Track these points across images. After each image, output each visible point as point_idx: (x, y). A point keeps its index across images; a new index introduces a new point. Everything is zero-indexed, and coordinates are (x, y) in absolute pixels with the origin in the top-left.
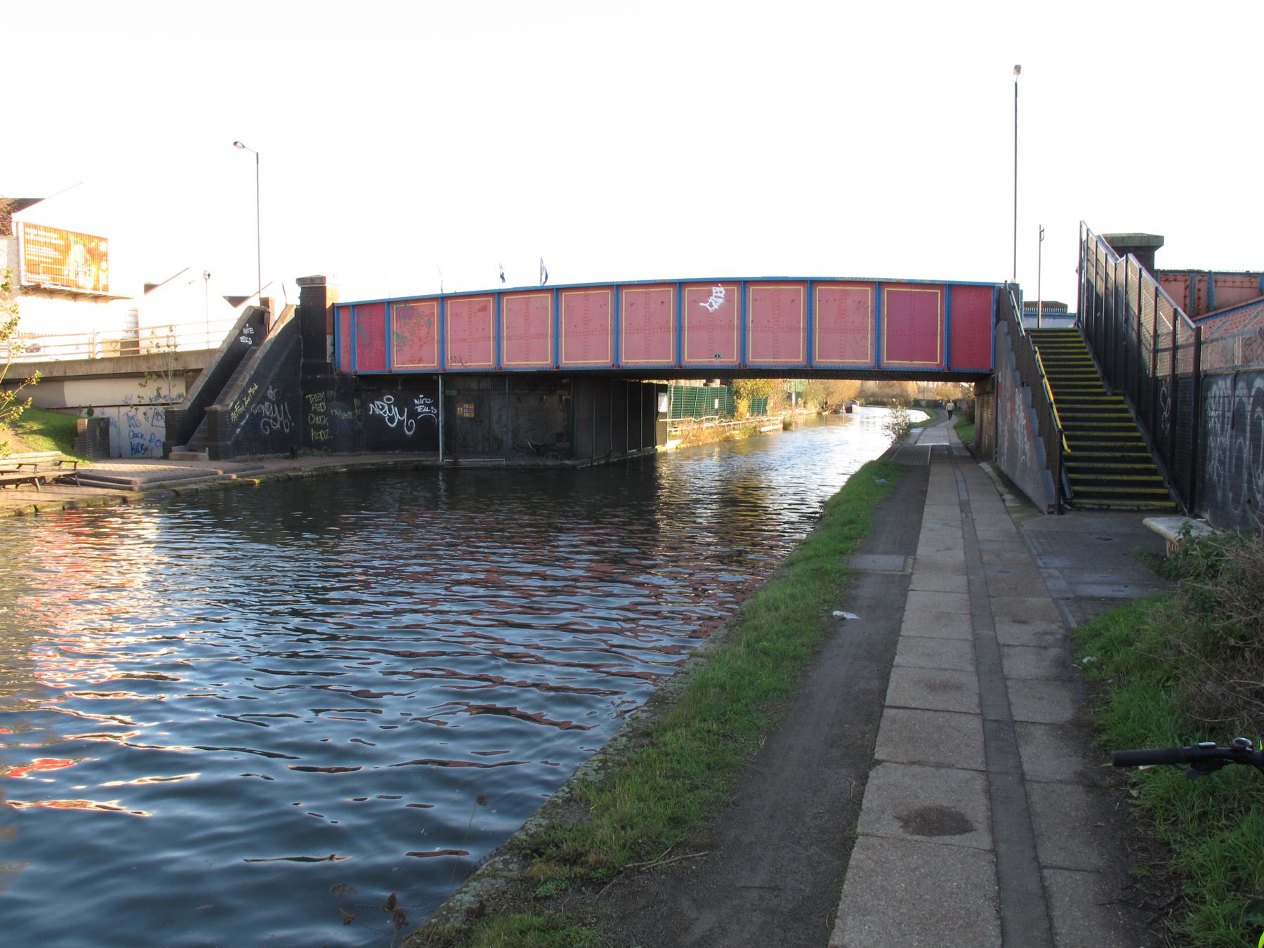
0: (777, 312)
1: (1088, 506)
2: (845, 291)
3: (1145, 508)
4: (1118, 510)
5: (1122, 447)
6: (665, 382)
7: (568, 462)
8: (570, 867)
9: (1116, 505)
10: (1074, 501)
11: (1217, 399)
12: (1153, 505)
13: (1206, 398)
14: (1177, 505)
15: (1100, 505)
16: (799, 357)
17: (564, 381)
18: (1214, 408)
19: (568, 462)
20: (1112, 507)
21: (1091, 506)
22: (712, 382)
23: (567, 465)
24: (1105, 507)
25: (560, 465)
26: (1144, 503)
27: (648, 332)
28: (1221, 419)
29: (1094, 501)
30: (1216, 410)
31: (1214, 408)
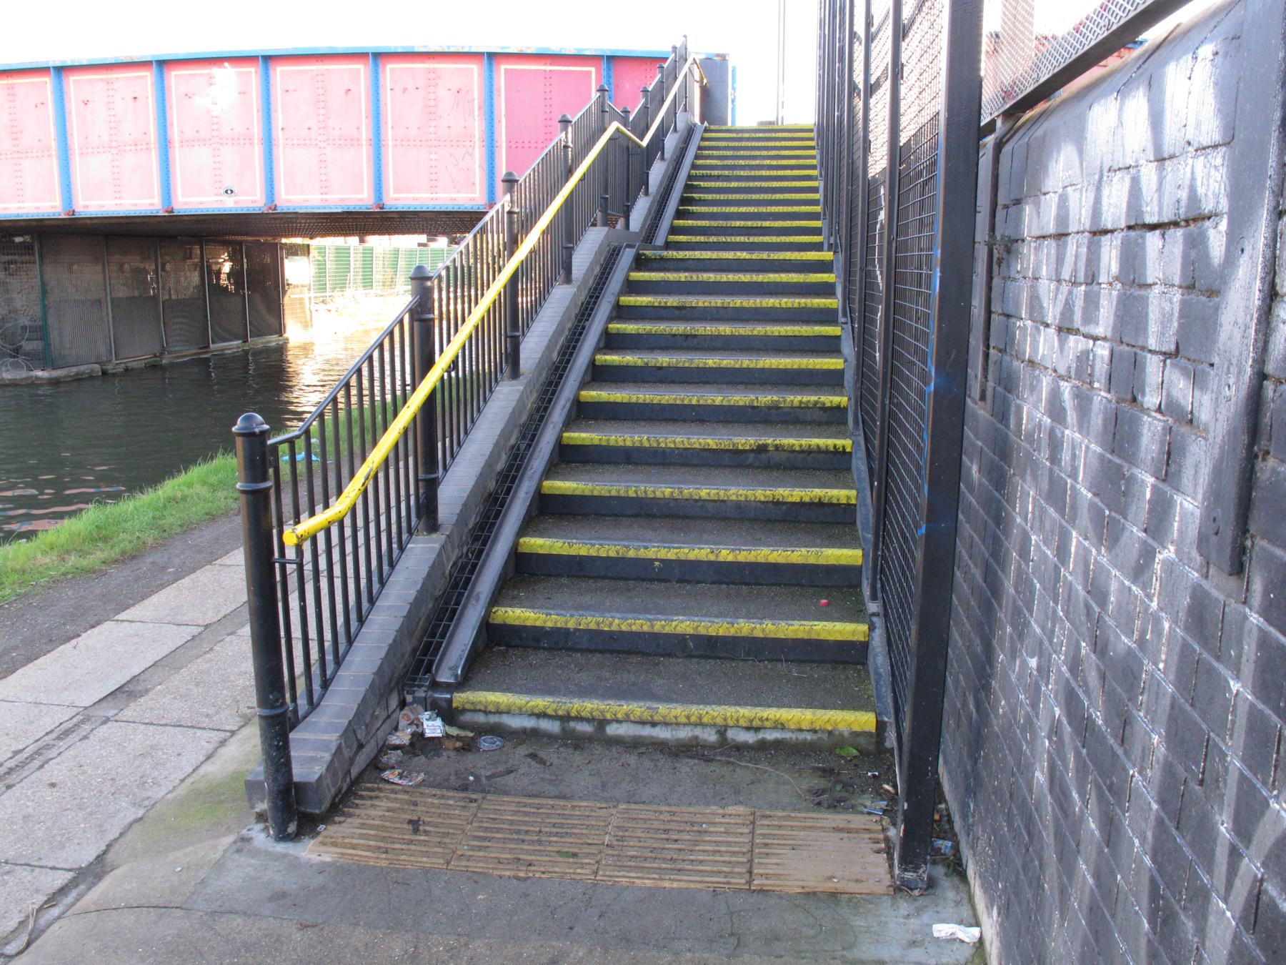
0: (322, 112)
1: (516, 723)
2: (434, 71)
3: (750, 738)
4: (635, 745)
5: (775, 408)
6: (307, 241)
7: (40, 373)
8: (385, 770)
9: (627, 719)
10: (460, 698)
11: (1075, 248)
12: (781, 726)
13: (1011, 245)
14: (881, 726)
15: (566, 718)
16: (361, 191)
17: (18, 240)
18: (1052, 314)
19: (40, 373)
20: (612, 730)
21: (530, 723)
22: (434, 240)
23: (37, 378)
24: (586, 728)
25: (27, 378)
26: (745, 712)
27: (114, 151)
28: (1101, 397)
29: (540, 702)
30: (1065, 330)
31: (1052, 314)
